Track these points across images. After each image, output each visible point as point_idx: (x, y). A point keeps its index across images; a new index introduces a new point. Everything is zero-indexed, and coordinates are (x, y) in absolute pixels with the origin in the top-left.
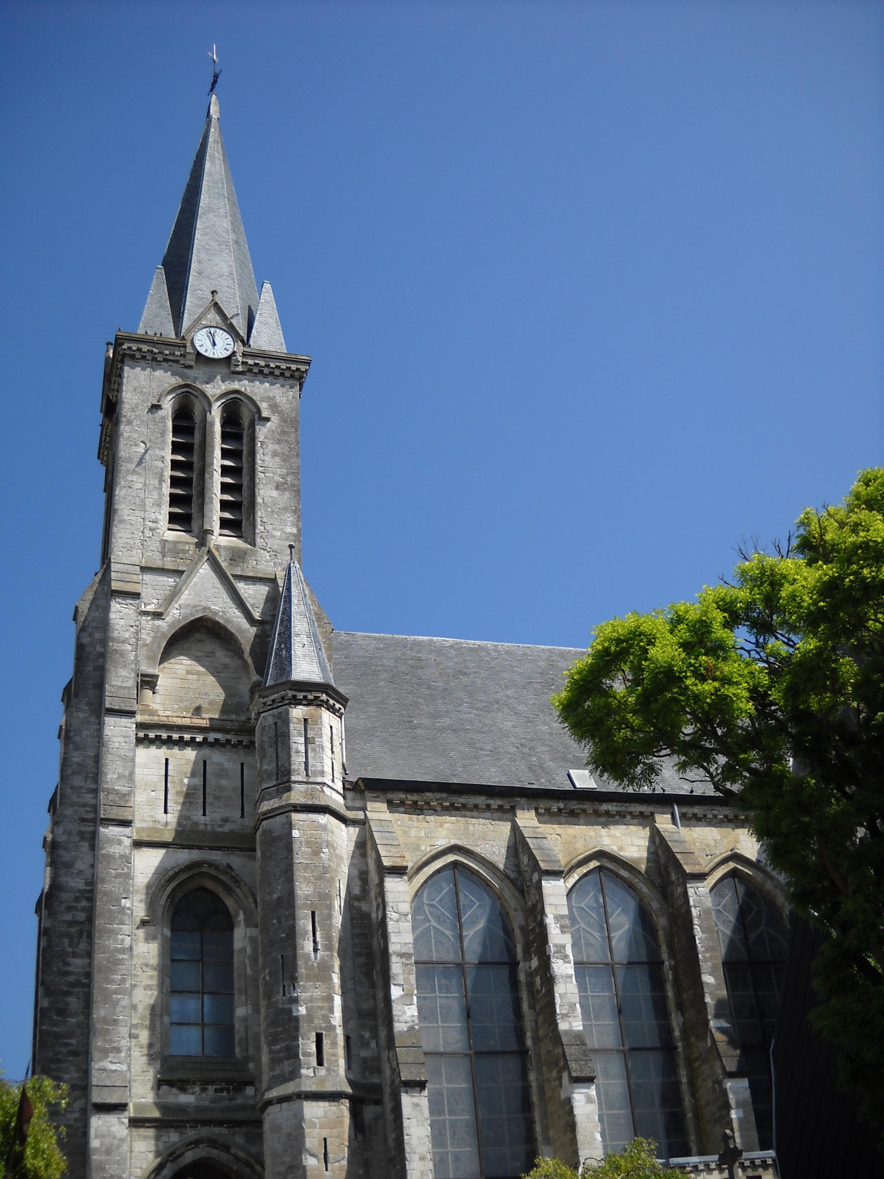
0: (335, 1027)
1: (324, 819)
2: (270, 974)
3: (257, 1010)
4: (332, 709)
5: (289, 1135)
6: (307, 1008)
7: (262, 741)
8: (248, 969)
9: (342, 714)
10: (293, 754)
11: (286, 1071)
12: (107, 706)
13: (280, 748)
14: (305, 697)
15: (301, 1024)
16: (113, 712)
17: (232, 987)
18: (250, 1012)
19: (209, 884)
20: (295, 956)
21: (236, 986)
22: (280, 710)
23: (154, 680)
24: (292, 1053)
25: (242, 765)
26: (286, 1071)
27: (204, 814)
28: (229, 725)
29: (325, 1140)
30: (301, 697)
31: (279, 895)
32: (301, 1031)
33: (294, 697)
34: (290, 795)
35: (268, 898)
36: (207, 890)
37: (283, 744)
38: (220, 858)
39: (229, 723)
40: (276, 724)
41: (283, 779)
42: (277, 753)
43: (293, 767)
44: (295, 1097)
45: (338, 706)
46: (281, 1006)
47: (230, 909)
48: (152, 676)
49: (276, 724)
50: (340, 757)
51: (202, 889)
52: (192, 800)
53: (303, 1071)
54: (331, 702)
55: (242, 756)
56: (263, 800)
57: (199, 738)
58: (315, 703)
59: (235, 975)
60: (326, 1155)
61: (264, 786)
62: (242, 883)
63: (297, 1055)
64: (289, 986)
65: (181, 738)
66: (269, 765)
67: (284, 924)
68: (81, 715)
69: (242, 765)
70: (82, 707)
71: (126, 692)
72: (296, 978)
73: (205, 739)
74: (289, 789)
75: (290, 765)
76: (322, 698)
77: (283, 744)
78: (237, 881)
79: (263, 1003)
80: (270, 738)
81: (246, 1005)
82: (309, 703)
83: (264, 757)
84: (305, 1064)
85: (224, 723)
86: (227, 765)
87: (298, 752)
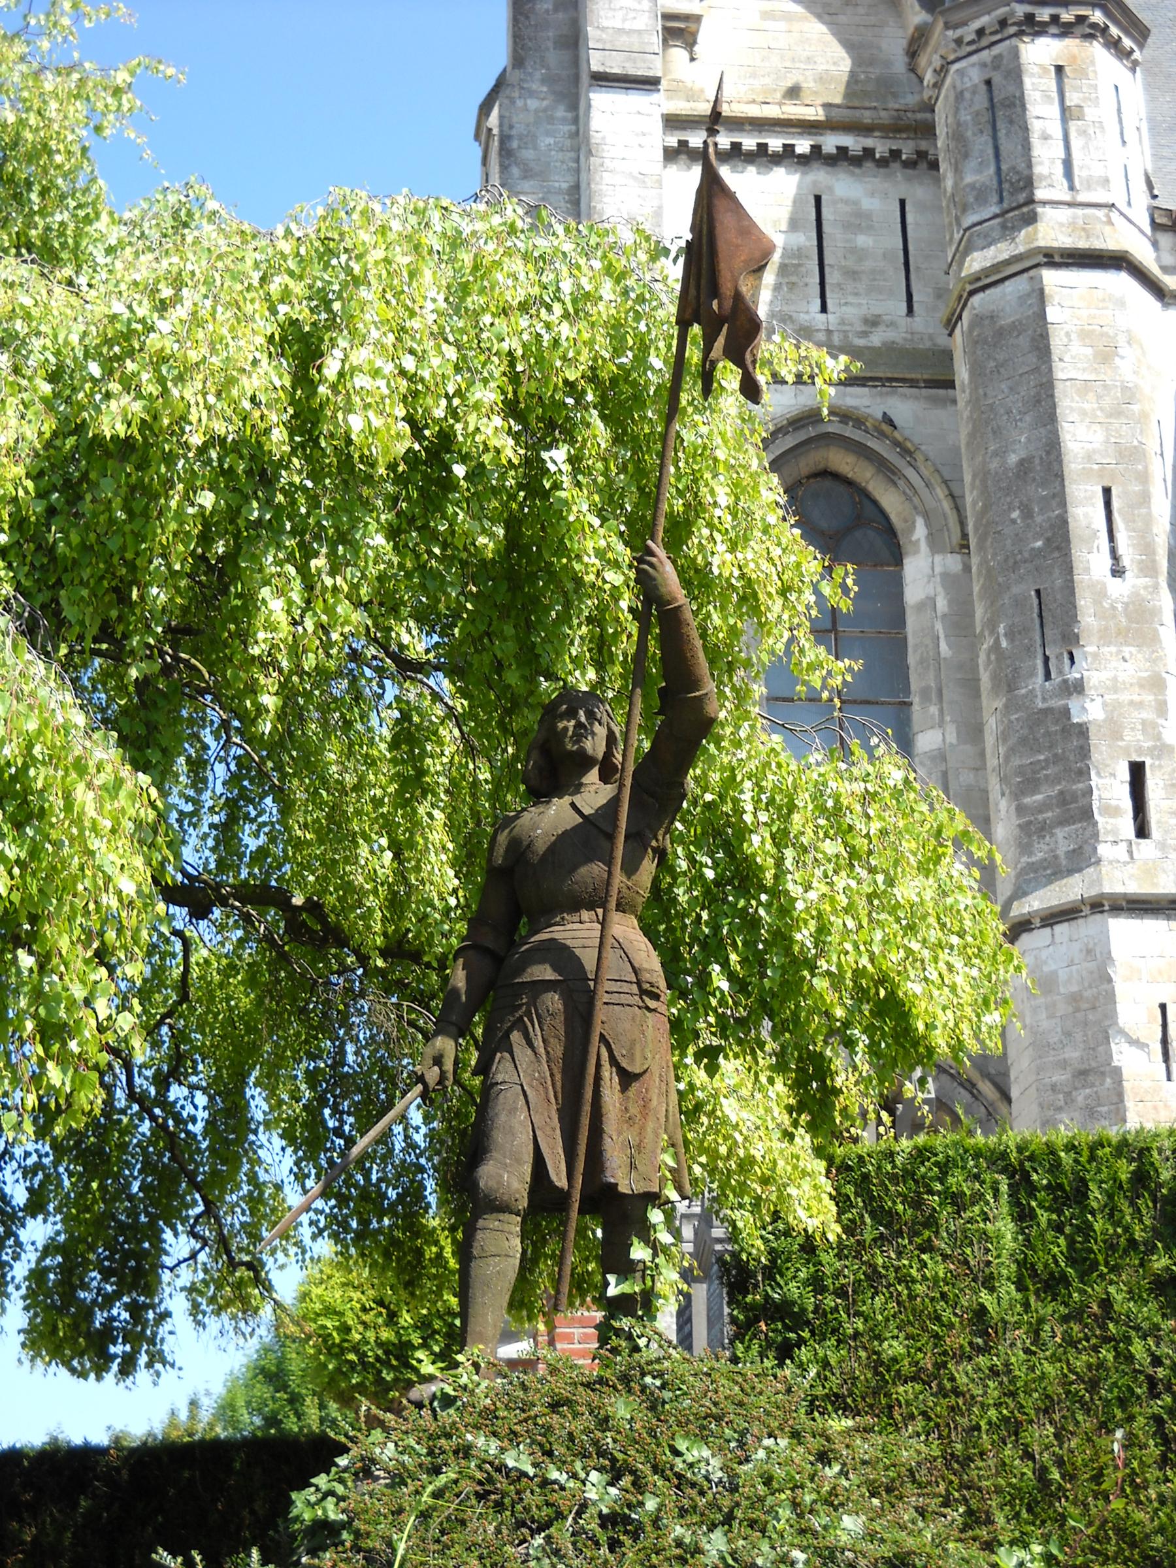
0: (916, 1147)
1: (1121, 281)
2: (1010, 635)
3: (973, 732)
4: (1114, 45)
5: (1075, 999)
6: (1105, 705)
7: (959, 124)
8: (943, 647)
9: (1135, 63)
10: (1035, 141)
11: (1062, 851)
12: (595, 67)
13: (1002, 134)
14: (1055, 19)
15: (1093, 741)
16: (604, 79)
17: (907, 690)
18: (952, 738)
19: (843, 462)
20: (1069, 588)
21: (915, 684)
22: (996, 50)
23: (693, 26)
24: (1078, 811)
25: (902, 203)
26: (1062, 851)
27: (824, 309)
28: (867, 117)
29: (1163, 1007)
30: (1046, 18)
31: (1023, 454)
32: (1095, 756)
33: (1030, 18)
34: (1036, 231)
35: (994, 465)
36: (836, 476)
37: (1011, 122)
38: (866, 401)
39: (867, 113)
40: (988, 83)
41: (1017, 200)
42: (996, 149)
43: (1038, 170)
44: (1086, 910)
45: (1127, 43)
46: (1041, 705)
47: (893, 517)
48: (686, 18)
49: (988, 83)
50: (1139, 157)
51: (826, 474)
52: (794, 279)
53: (1103, 850)
54: (1114, 31)
55: (898, 184)
56: (967, 251)
57: (803, 146)
58: (1079, 30)
59: (912, 659)
60: (1165, 1042)
61: (968, 220)
62: (919, 457)
63: (1087, 814)
64: (1059, 657)
65: (763, 147)
66: (980, 172)
67: (1039, 519)
68: (533, 104)
69: (902, 203)
70: (534, 87)
71: (634, 39)
72: (1077, 637)
73: (816, 149)
74: (1032, 219)
75: (1030, 166)
76: (1093, 19)
77: (1011, 122)
78: (906, 452)
79: (992, 707)
80: (977, 114)
81: (941, 724)
82: (1066, 30)
83: (966, 156)
84: (1107, 832)
85: (857, 113)
86: (870, 204)
87: (1046, 137)
